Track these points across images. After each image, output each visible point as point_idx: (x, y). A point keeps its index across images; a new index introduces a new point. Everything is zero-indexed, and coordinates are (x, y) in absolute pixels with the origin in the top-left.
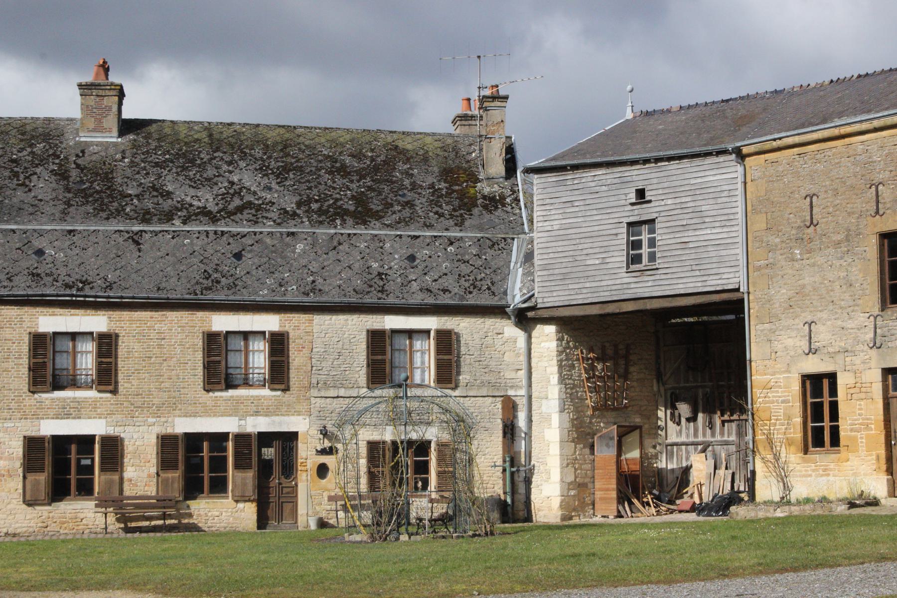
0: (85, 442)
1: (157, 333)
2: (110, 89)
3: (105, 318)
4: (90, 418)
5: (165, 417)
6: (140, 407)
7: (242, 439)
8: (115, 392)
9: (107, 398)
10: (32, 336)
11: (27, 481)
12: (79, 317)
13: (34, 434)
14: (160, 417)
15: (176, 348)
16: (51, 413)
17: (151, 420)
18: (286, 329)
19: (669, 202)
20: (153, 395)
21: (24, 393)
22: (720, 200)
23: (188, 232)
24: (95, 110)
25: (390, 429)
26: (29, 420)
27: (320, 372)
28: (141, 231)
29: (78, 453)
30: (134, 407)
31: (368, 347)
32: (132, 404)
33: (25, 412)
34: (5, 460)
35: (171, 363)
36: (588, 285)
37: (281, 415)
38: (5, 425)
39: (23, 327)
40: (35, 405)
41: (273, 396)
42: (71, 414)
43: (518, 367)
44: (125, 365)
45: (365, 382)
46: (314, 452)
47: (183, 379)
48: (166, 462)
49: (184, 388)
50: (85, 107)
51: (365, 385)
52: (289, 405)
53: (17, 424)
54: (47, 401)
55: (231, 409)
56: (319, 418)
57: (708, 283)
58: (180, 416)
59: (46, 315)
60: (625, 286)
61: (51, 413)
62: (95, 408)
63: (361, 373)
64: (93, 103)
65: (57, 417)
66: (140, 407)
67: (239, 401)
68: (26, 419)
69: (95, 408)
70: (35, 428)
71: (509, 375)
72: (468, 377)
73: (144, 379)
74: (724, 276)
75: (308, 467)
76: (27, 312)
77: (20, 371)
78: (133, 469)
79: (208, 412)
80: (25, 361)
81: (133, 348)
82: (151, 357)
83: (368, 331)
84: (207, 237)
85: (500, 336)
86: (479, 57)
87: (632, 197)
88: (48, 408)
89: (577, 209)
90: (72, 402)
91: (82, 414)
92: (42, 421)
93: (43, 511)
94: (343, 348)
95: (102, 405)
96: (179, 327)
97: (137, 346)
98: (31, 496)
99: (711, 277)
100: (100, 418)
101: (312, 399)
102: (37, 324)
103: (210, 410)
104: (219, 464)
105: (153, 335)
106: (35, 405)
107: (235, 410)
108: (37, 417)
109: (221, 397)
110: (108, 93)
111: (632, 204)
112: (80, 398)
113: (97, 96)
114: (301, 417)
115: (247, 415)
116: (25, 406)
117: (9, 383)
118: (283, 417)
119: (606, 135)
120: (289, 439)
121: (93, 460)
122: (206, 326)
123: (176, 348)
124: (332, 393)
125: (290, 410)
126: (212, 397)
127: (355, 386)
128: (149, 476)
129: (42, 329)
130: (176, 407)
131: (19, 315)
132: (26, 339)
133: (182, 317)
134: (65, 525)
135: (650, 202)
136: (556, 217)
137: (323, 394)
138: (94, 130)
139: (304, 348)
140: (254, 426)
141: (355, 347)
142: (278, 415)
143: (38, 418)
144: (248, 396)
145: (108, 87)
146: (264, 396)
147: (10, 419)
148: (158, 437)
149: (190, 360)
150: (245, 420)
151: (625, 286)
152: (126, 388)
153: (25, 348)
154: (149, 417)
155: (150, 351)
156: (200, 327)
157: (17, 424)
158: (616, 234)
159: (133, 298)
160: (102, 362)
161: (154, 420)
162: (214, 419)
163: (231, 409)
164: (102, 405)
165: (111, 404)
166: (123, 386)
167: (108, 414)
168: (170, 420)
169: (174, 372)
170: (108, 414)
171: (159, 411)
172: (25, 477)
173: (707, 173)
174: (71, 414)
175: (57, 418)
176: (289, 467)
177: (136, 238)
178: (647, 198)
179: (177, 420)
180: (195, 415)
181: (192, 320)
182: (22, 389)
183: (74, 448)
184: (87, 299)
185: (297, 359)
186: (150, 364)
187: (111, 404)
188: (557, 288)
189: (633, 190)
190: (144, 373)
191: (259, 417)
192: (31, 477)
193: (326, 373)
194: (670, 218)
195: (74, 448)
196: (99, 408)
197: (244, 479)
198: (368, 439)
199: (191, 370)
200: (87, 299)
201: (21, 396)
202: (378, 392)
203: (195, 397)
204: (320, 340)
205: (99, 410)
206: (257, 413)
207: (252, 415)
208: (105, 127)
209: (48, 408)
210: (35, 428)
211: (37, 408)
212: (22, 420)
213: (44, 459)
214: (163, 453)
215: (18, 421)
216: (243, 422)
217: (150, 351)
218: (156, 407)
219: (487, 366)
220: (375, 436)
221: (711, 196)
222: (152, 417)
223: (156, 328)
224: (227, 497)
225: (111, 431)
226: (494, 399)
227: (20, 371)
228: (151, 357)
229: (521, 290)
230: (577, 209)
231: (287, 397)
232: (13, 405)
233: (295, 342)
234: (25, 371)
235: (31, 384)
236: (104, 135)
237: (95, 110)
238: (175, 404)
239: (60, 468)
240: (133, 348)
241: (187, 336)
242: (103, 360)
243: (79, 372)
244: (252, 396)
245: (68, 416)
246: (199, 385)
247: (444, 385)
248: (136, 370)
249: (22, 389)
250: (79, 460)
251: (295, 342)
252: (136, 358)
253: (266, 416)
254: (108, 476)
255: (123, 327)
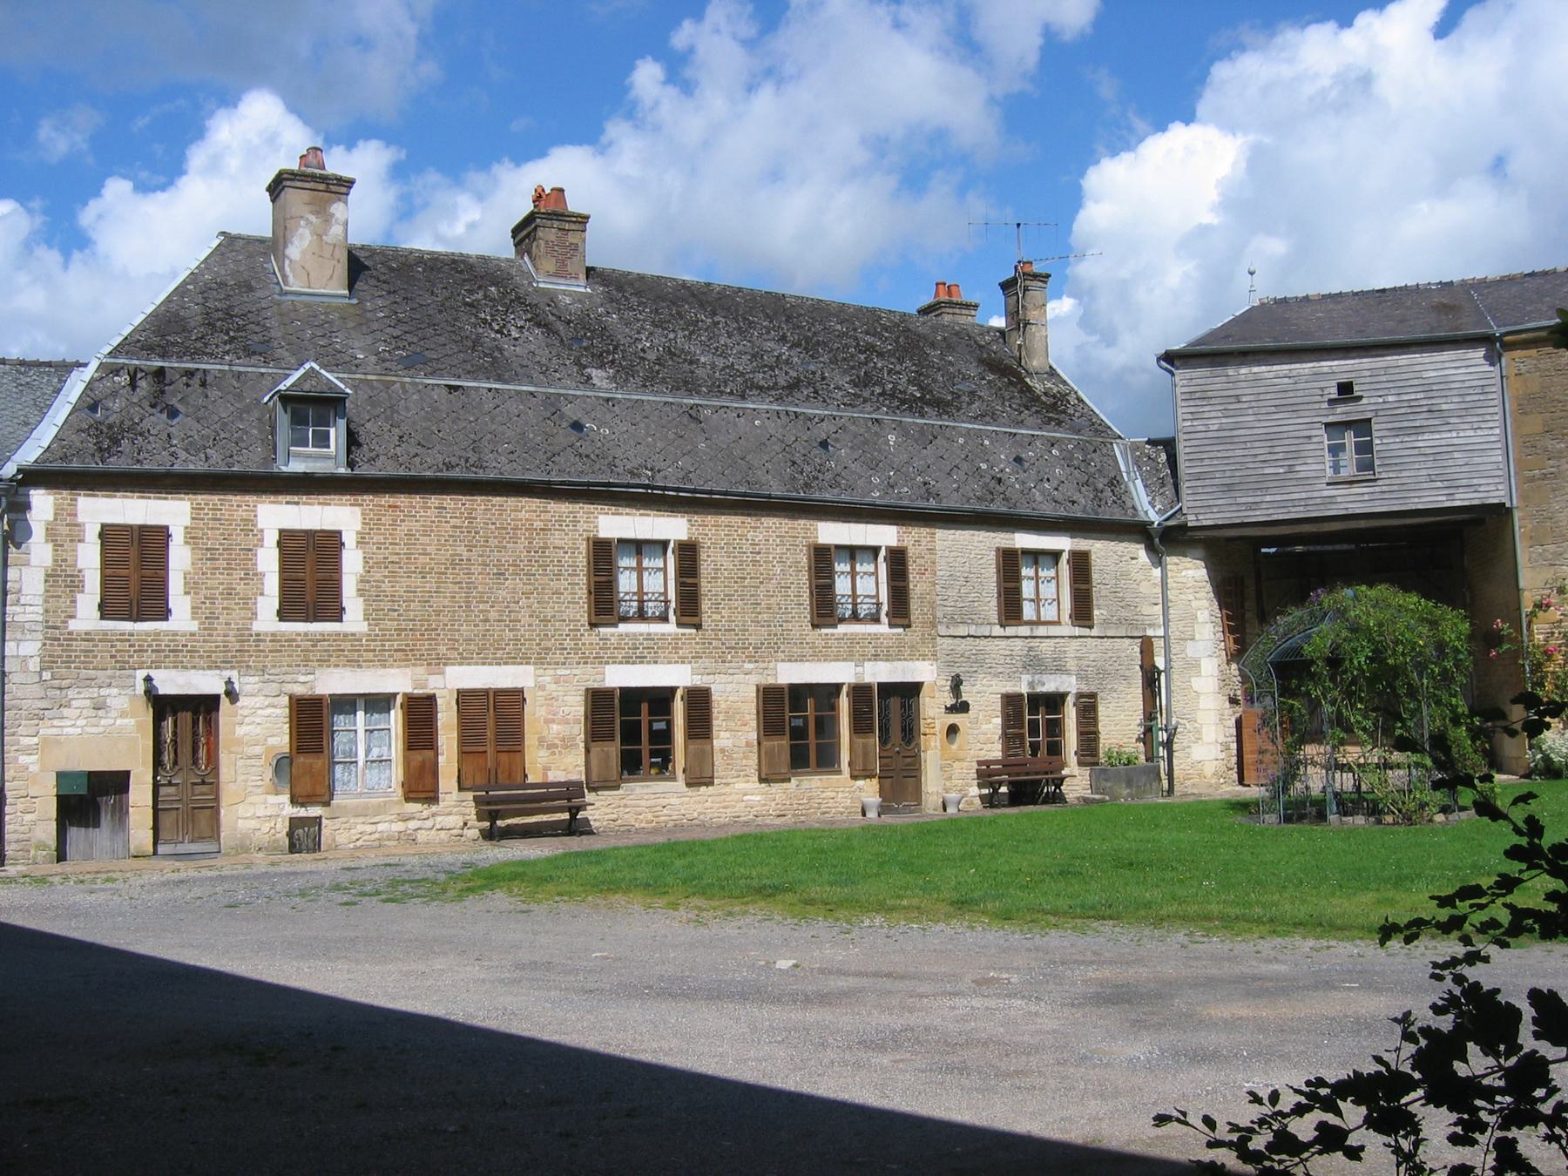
0: (660, 699)
1: (751, 544)
2: (574, 222)
3: (685, 519)
4: (669, 663)
5: (764, 662)
6: (733, 648)
7: (860, 692)
8: (698, 627)
9: (691, 634)
10: (591, 542)
11: (592, 754)
12: (651, 518)
13: (596, 685)
14: (756, 661)
15: (774, 566)
16: (620, 656)
17: (748, 666)
18: (905, 544)
19: (1390, 399)
20: (748, 630)
21: (582, 625)
22: (1468, 398)
23: (754, 410)
24: (556, 248)
25: (1026, 678)
26: (589, 666)
27: (945, 603)
28: (697, 405)
29: (650, 714)
30: (727, 648)
31: (998, 571)
32: (723, 644)
33: (584, 653)
34: (559, 724)
35: (771, 587)
36: (1268, 498)
37: (905, 659)
38: (559, 672)
39: (578, 531)
40: (598, 644)
41: (893, 634)
42: (646, 657)
43: (1155, 601)
44: (801, 583)
45: (997, 617)
46: (943, 710)
47: (786, 609)
48: (596, 730)
49: (787, 621)
50: (1230, 127)
51: (997, 621)
52: (913, 647)
53: (575, 672)
54: (612, 638)
55: (845, 652)
56: (949, 664)
57: (1457, 496)
58: (783, 661)
59: (607, 514)
60: (1328, 500)
61: (620, 656)
62: (677, 648)
63: (991, 604)
64: (553, 238)
65: (627, 661)
66: (733, 648)
67: (853, 639)
68: (586, 663)
69: (677, 648)
70: (599, 677)
71: (1146, 610)
72: (1105, 613)
73: (736, 608)
74: (1482, 489)
75: (937, 729)
76: (581, 509)
77: (575, 594)
78: (727, 734)
79: (820, 655)
80: (582, 579)
81: (722, 565)
82: (745, 578)
83: (998, 549)
84: (779, 417)
85: (1134, 562)
86: (1018, 225)
87: (1333, 393)
88: (615, 648)
89: (1246, 405)
90: (647, 639)
91: (660, 657)
92: (607, 666)
93: (776, 788)
94: (970, 572)
95: (684, 644)
96: (777, 537)
97: (727, 564)
98: (599, 777)
99: (1461, 490)
100: (683, 662)
101: (938, 638)
102: (597, 527)
103: (821, 652)
104: (826, 726)
105: (747, 547)
106: (598, 644)
107: (852, 651)
108: (600, 660)
109: (833, 635)
110: (573, 227)
111: (1331, 402)
112: (656, 634)
113: (559, 229)
114: (927, 663)
115: (864, 660)
116: (584, 644)
117: (561, 612)
118: (905, 663)
119: (1236, 321)
120: (910, 691)
121: (670, 724)
122: (810, 538)
123: (774, 566)
124: (962, 631)
125: (915, 654)
126: (819, 635)
127: (986, 622)
128: (748, 744)
129: (603, 534)
130: (779, 648)
131: (571, 512)
132: (583, 547)
133: (781, 524)
134: (641, 817)
135: (1360, 398)
136: (1213, 414)
137: (952, 632)
138: (556, 275)
139: (926, 570)
140: (874, 674)
141: (983, 571)
142: (900, 660)
143: (601, 663)
144: (864, 634)
145: (574, 219)
146: (882, 635)
147: (564, 664)
148: (758, 690)
149: (792, 583)
150: (863, 666)
151: (1328, 500)
152: (715, 621)
153: (582, 560)
154: (744, 662)
155: (743, 569)
156: (804, 538)
157: (575, 672)
158: (1309, 437)
159: (726, 493)
160: (684, 583)
161: (751, 666)
162: (826, 664)
163: (845, 652)
164: (684, 644)
165: (697, 643)
166: (706, 621)
167: (693, 658)
168: (772, 665)
169: (773, 600)
170: (693, 658)
171: (760, 653)
172: (587, 751)
173: (1447, 365)
174: (646, 657)
175: (627, 663)
176: (910, 731)
177: (693, 412)
178: (1356, 394)
179: (780, 665)
180: (801, 659)
181: (794, 528)
182: (579, 621)
183: (645, 707)
184: (681, 494)
185: (917, 585)
186: (744, 587)
187: (697, 643)
188: (1220, 502)
189: (1334, 383)
190: (737, 600)
191: (879, 663)
192: (596, 749)
193: (952, 604)
194: (1394, 418)
195: (645, 707)
196: (682, 648)
197: (865, 746)
198: (1004, 691)
199: (795, 596)
200: (681, 494)
201: (579, 630)
202: (1010, 631)
203: (801, 635)
204: (944, 560)
205: (681, 652)
206: (876, 657)
207: (869, 660)
208: (570, 271)
209: (615, 648)
210: (599, 677)
211: (600, 648)
212: (581, 665)
213: (613, 722)
214: (765, 711)
215: (575, 666)
216: (859, 669)
217: (743, 569)
218: (754, 648)
219: (1123, 599)
220: (1010, 688)
221: (1455, 392)
222: (750, 662)
223: (749, 537)
224: (839, 772)
225: (698, 681)
226: (1131, 640)
227: (575, 594)
228: (745, 578)
229: (1152, 504)
230: (1246, 405)
231: (912, 636)
232: (568, 643)
233: (915, 562)
234: (582, 593)
235: (593, 612)
236: (568, 282)
237: (556, 248)
238: (776, 643)
239: (631, 734)
240: (722, 565)
241: (787, 550)
242: (685, 579)
243: (645, 598)
244: (869, 634)
245: (641, 659)
246: (805, 617)
247: (1082, 623)
248: (727, 595)
249: (579, 621)
250: (650, 723)
251: (915, 562)
252: (725, 578)
253: (887, 660)
254: (695, 746)
255: (707, 535)
